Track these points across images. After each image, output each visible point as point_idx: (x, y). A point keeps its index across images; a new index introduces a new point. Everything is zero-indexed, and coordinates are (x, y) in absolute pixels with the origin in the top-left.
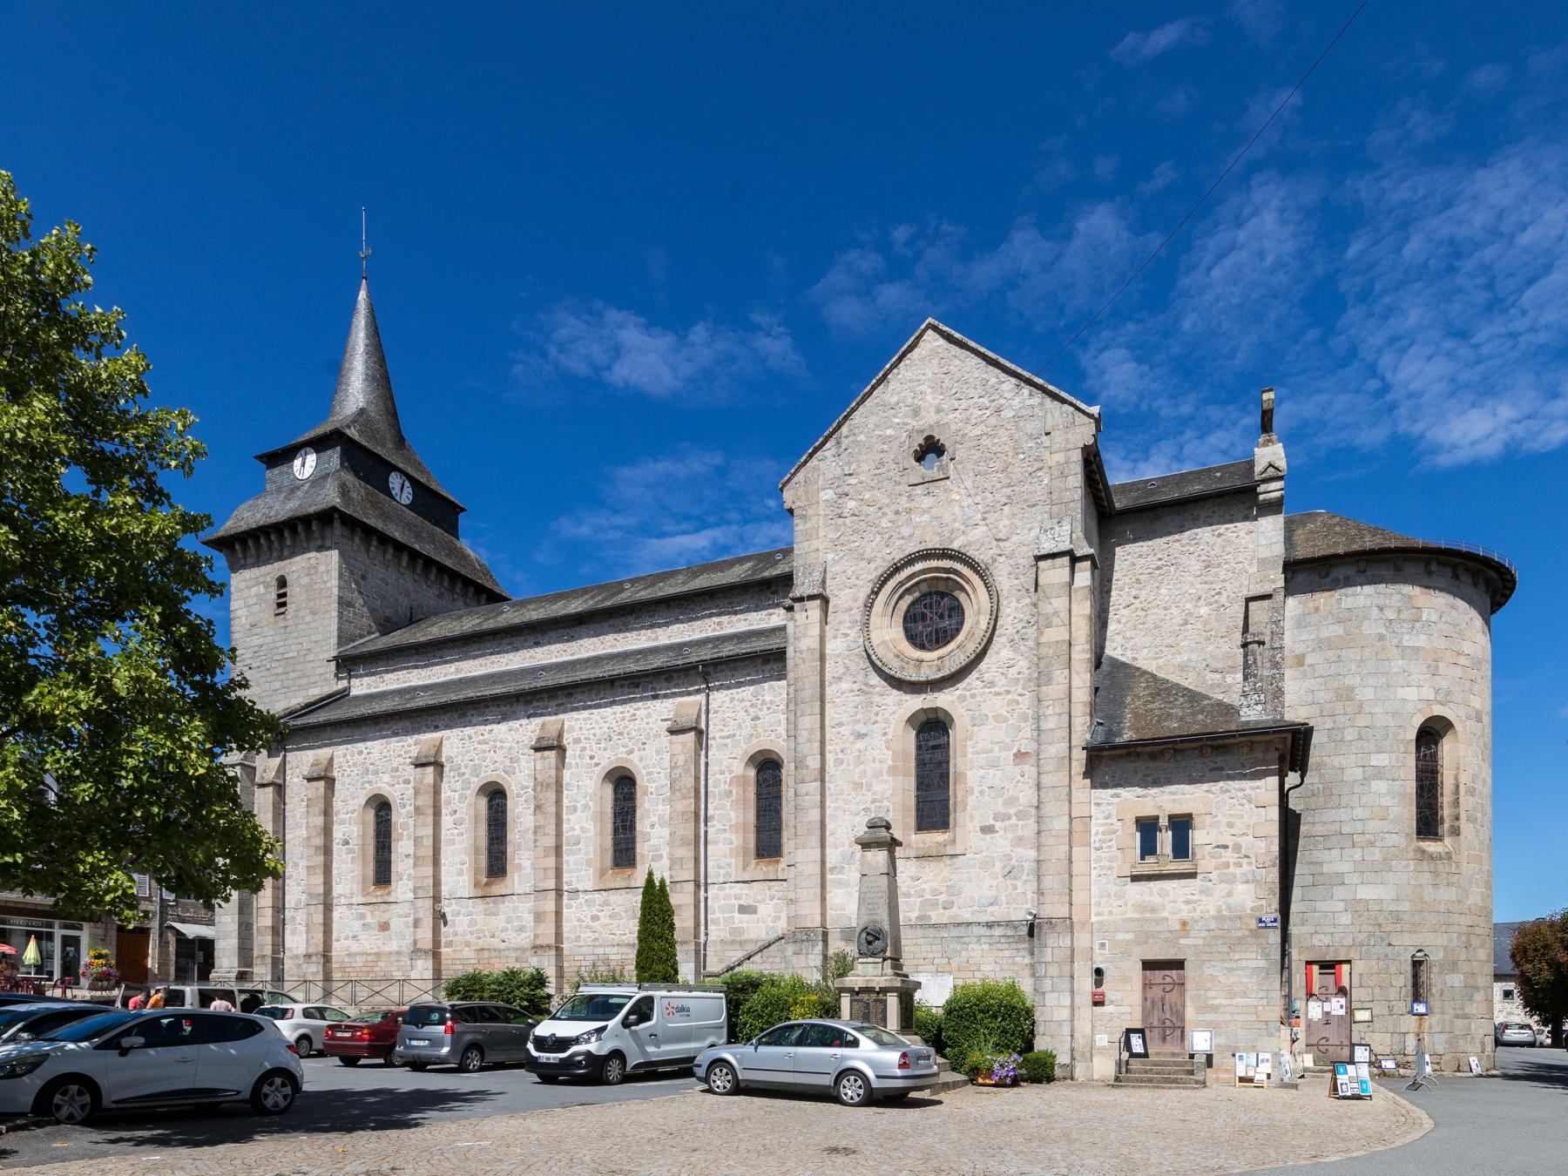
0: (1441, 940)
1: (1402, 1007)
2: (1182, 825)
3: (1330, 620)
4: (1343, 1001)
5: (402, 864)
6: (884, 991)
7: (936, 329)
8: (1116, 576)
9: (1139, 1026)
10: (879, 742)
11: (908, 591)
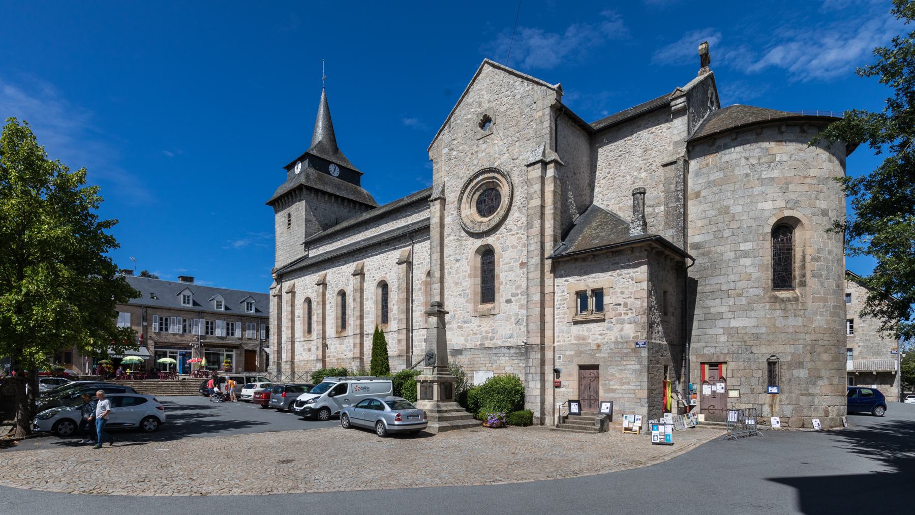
0: (789, 349)
1: (760, 389)
2: (599, 294)
3: (715, 170)
4: (723, 385)
5: (352, 321)
6: (432, 382)
7: (488, 63)
8: (599, 163)
9: (576, 398)
10: (464, 262)
11: (477, 190)
